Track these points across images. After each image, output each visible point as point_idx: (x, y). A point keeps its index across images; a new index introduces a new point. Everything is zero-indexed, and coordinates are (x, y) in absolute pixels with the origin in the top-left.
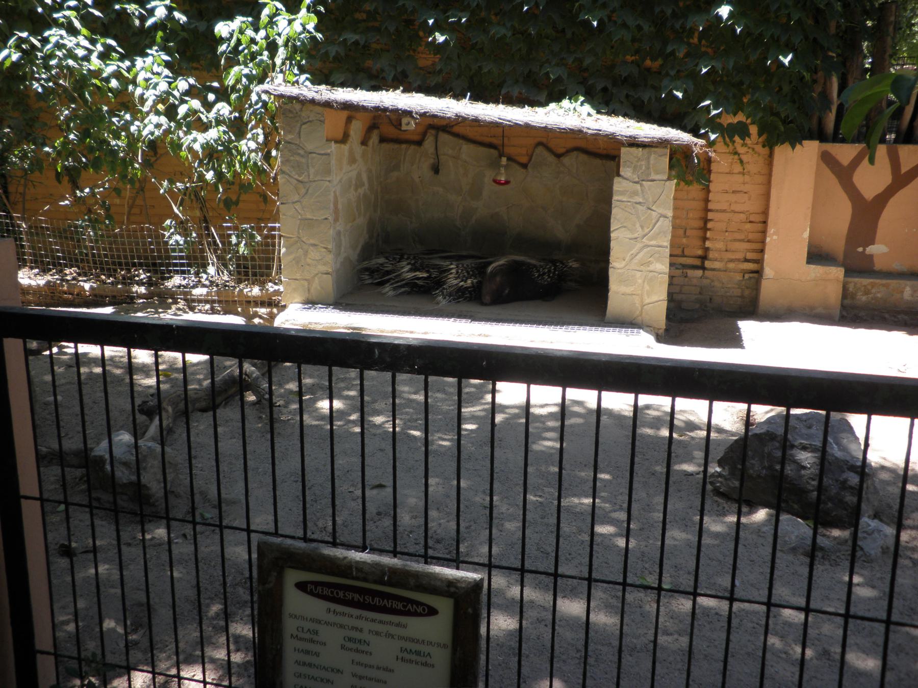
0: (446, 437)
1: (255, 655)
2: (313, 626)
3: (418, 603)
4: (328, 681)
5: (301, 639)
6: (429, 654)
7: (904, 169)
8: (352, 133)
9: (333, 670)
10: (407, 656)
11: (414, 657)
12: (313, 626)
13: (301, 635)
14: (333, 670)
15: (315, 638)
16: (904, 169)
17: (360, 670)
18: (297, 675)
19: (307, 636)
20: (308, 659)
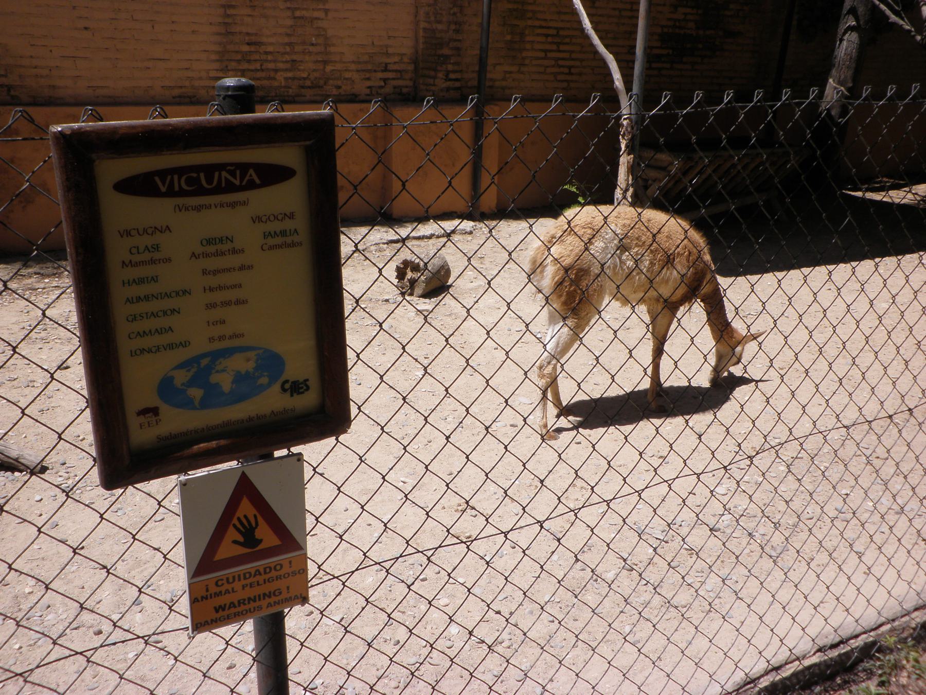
0: (632, 110)
1: (486, 76)
2: (148, 241)
3: (244, 167)
4: (173, 311)
5: (137, 264)
6: (295, 230)
7: (218, 557)
8: (860, 639)
9: (177, 294)
10: (271, 241)
11: (279, 240)
12: (148, 241)
13: (137, 258)
14: (177, 294)
15: (157, 256)
16: (218, 557)
17: (214, 281)
18: (130, 319)
19: (146, 256)
20: (143, 290)
